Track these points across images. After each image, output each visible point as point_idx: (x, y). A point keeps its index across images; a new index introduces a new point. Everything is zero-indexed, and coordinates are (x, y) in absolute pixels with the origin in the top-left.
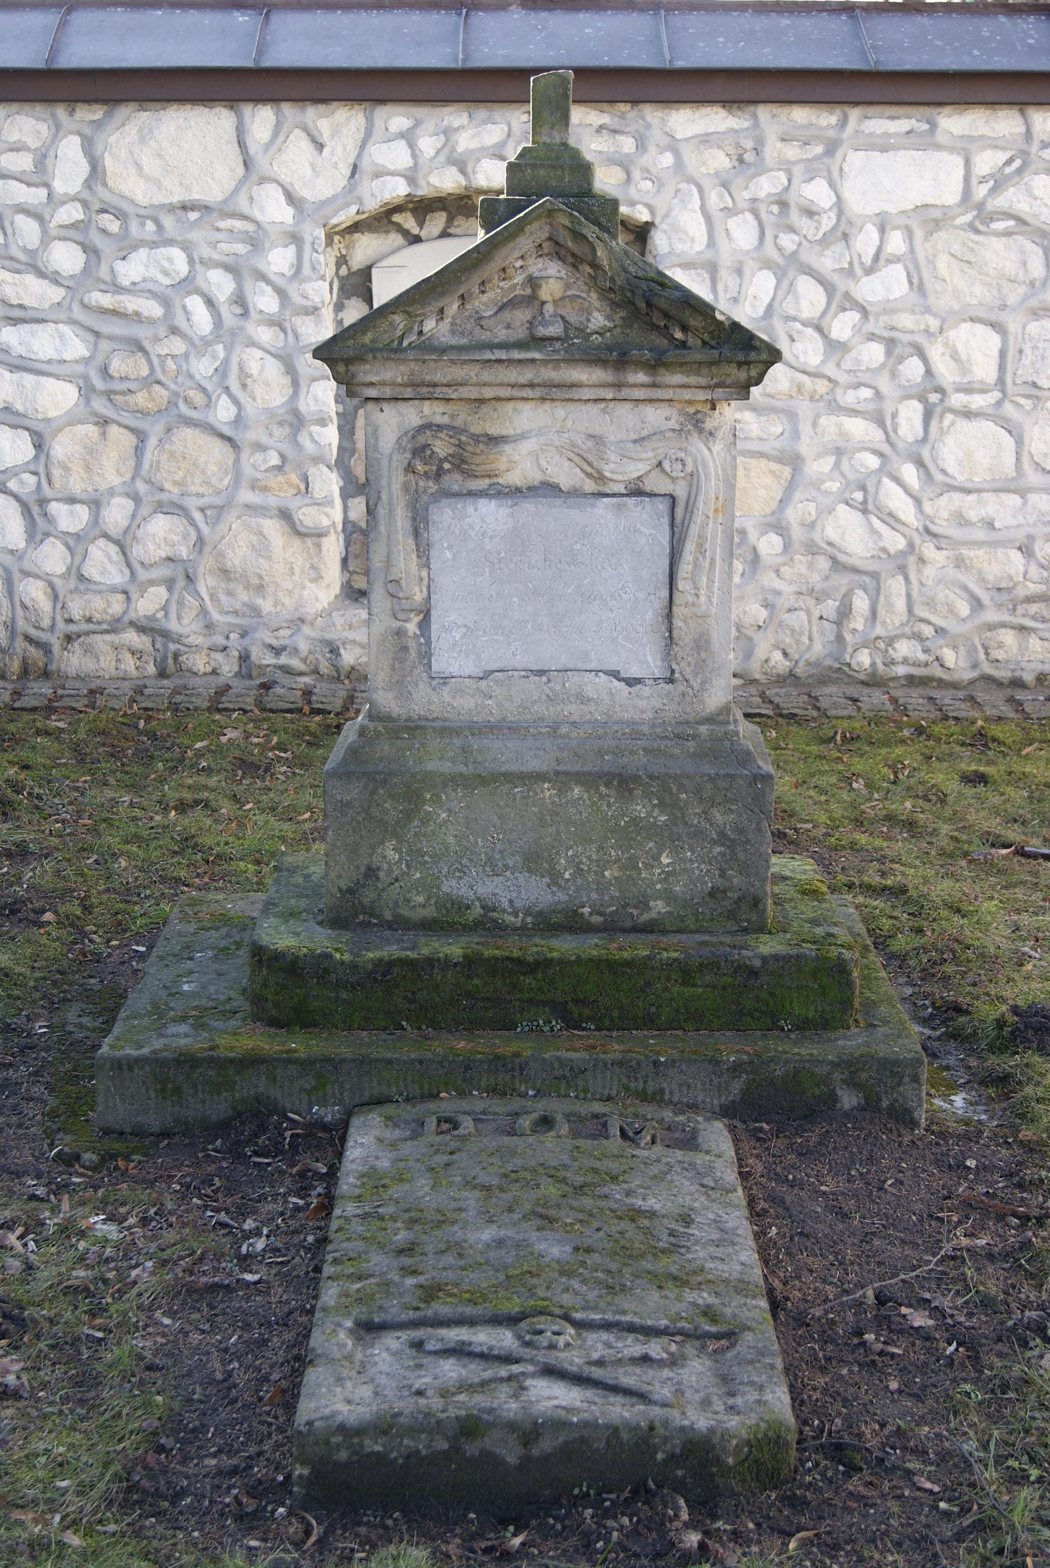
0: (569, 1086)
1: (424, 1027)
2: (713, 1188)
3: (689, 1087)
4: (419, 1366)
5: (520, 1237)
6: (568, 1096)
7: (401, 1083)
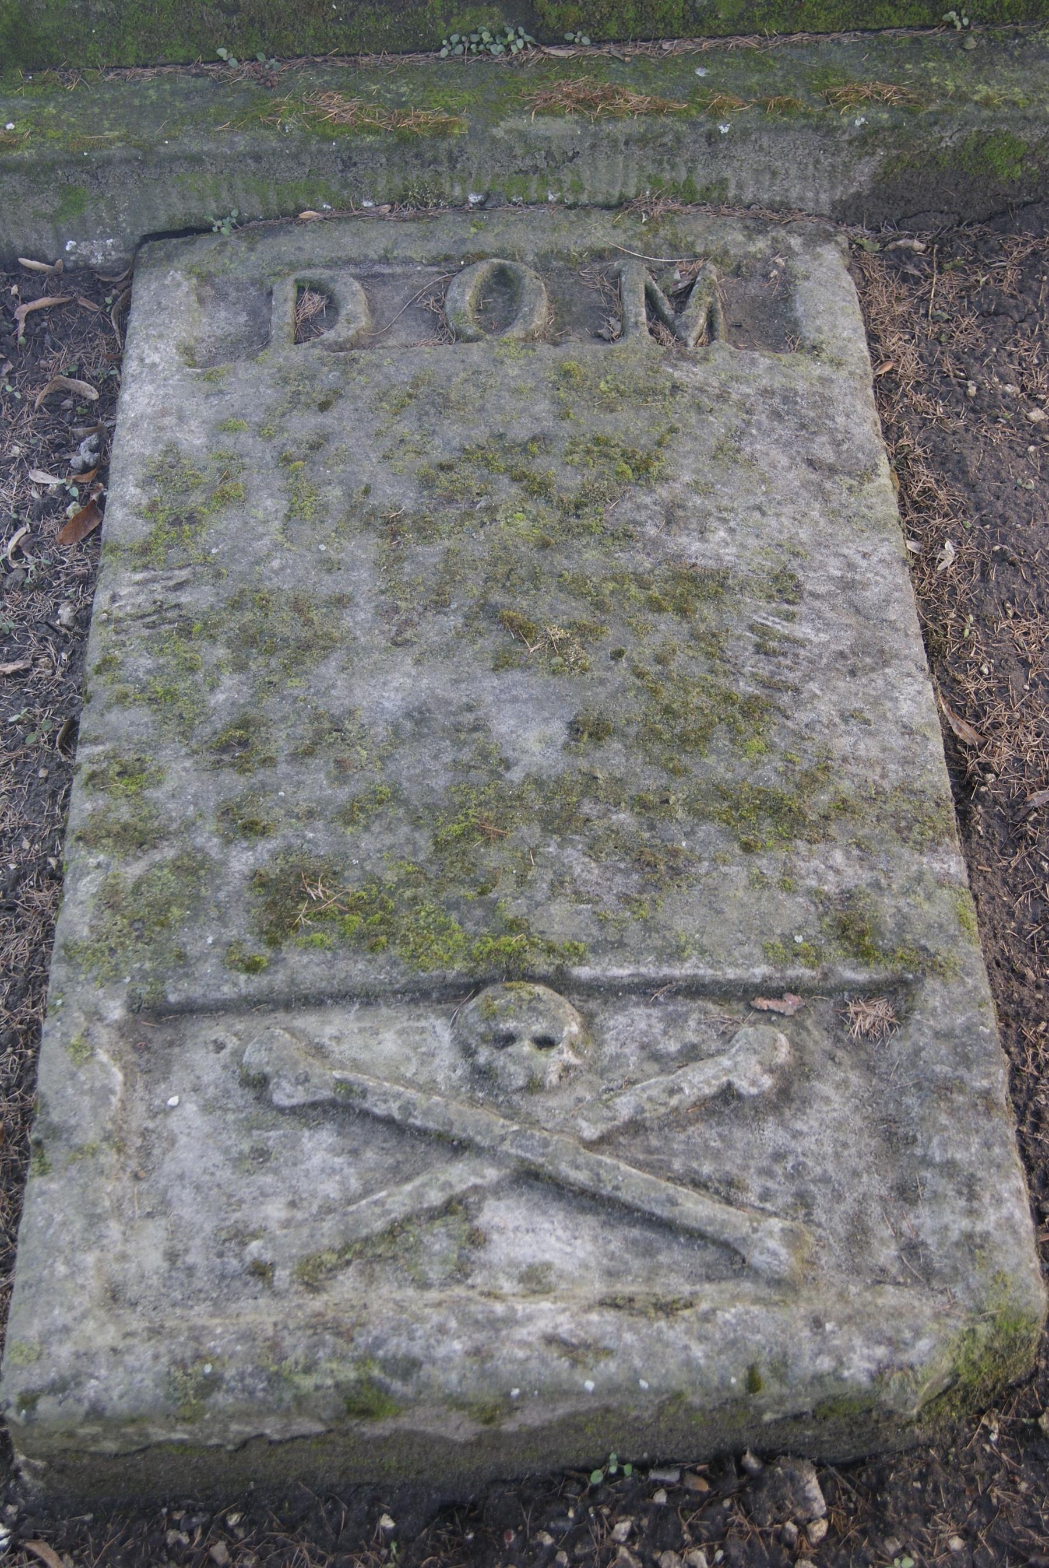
0: (544, 183)
1: (261, 57)
2: (832, 470)
3: (774, 174)
4: (262, 1154)
5: (459, 696)
6: (543, 202)
7: (224, 194)
